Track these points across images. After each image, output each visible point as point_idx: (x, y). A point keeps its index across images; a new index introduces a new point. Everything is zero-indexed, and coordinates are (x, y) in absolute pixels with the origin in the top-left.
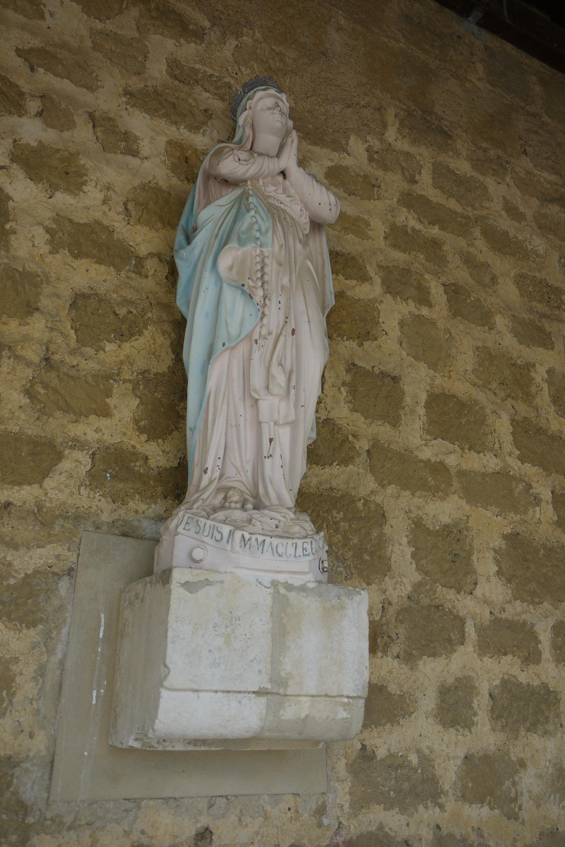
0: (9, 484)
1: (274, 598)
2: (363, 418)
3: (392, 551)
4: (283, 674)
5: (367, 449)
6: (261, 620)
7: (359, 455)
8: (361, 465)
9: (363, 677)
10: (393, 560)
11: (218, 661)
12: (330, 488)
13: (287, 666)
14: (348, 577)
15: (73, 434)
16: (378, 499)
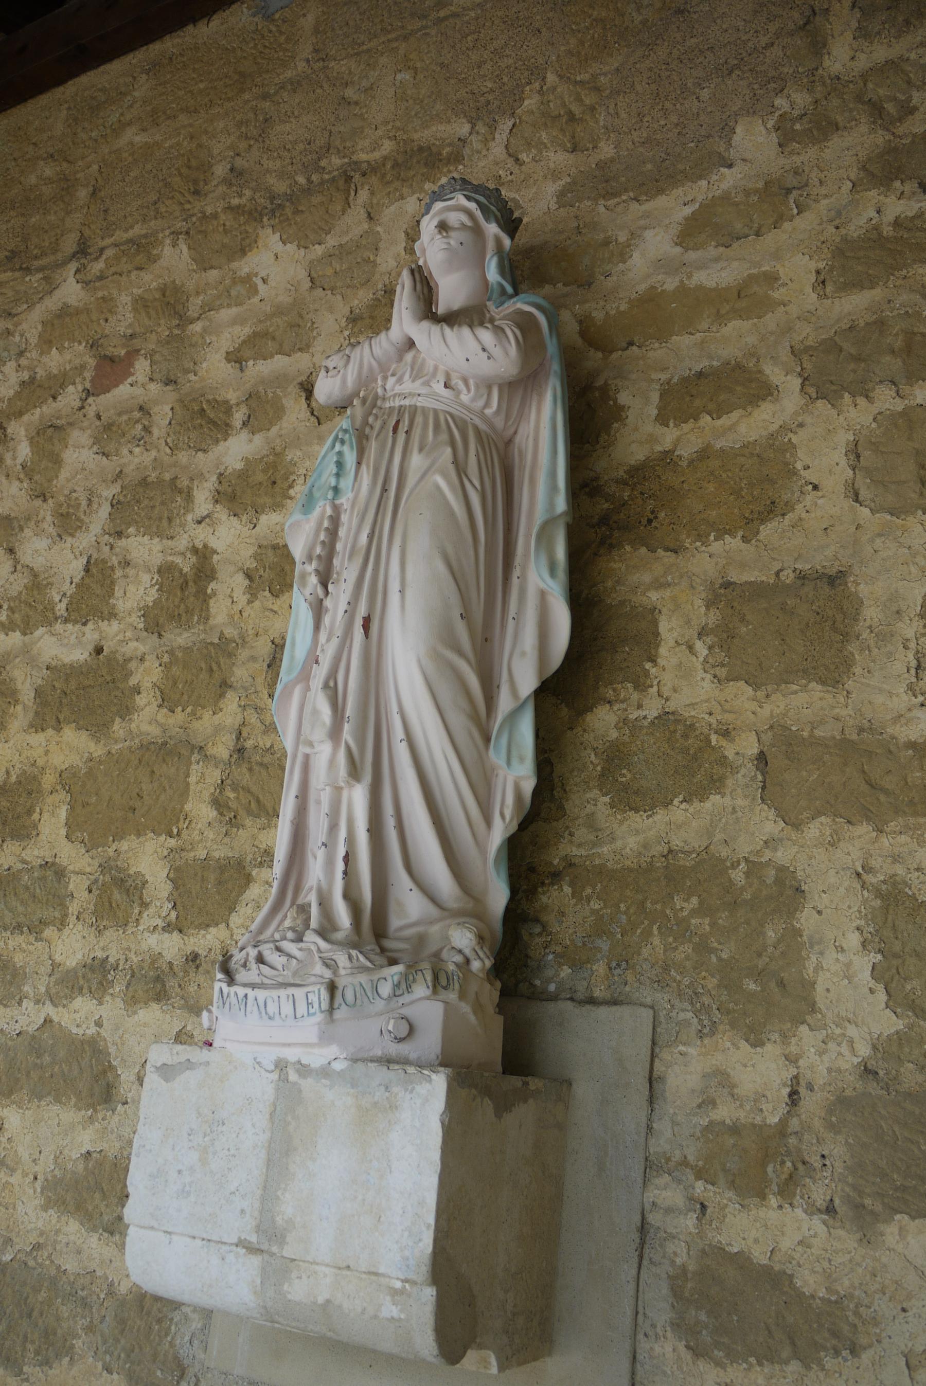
0: (196, 927)
1: (277, 1089)
2: (750, 689)
3: (819, 968)
4: (279, 1220)
5: (756, 751)
6: (253, 1125)
7: (735, 770)
8: (739, 790)
9: (421, 1244)
10: (820, 989)
11: (187, 1188)
12: (670, 851)
13: (287, 1208)
14: (706, 1031)
15: (265, 846)
16: (783, 856)
